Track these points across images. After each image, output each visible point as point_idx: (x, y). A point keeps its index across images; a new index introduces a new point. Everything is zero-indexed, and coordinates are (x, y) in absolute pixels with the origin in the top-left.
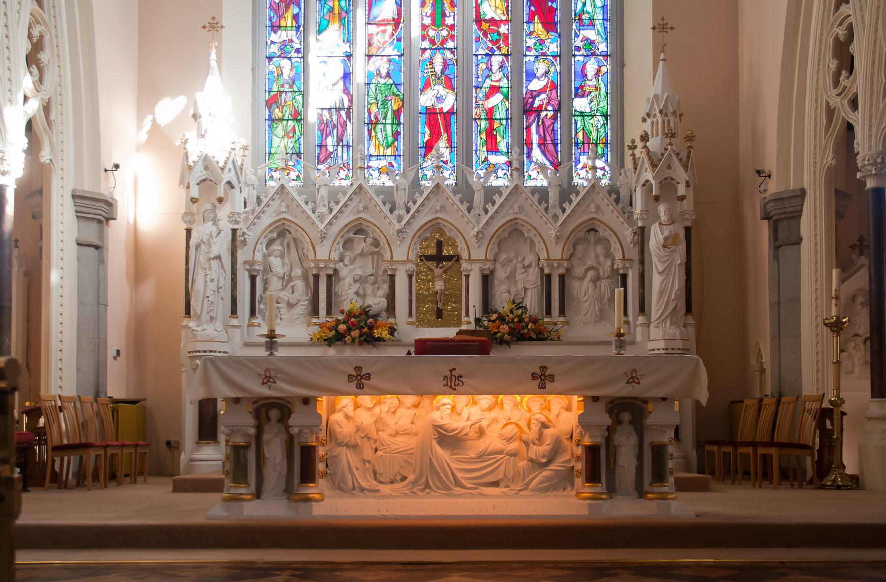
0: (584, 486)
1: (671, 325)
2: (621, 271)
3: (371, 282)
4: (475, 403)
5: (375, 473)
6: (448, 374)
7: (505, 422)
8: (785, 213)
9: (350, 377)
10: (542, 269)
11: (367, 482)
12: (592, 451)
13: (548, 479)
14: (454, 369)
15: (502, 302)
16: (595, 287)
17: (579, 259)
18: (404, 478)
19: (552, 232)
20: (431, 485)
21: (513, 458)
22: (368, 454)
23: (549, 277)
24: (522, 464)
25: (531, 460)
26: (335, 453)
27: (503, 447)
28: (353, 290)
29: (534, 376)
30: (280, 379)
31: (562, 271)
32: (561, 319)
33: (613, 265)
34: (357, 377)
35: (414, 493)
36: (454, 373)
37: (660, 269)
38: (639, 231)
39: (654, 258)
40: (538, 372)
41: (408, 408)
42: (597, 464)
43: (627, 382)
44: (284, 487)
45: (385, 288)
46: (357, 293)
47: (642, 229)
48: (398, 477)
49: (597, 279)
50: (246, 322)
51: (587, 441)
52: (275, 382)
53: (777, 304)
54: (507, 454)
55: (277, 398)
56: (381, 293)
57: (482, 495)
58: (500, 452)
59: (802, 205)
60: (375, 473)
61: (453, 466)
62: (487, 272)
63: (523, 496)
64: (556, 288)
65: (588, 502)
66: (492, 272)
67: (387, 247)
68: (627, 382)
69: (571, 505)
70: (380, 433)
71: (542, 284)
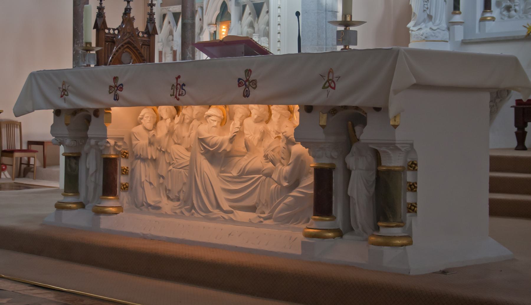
13: (289, 207)
20: (196, 206)
35: (182, 212)
50: (479, 16)
52: (67, 95)
54: (264, 175)
63: (266, 226)
68: (324, 87)
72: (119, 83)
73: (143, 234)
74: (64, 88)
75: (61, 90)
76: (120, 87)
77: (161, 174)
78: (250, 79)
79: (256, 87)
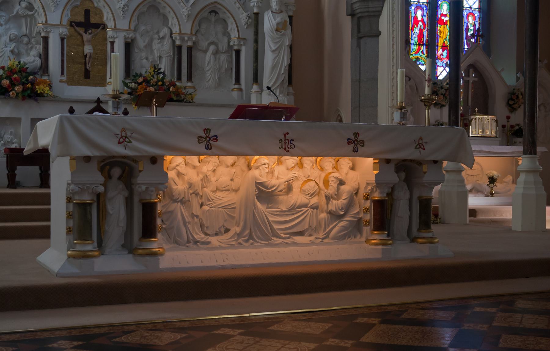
2: (236, 48)
3: (25, 42)
4: (280, 163)
5: (202, 226)
6: (282, 137)
7: (304, 179)
8: (368, 12)
9: (200, 138)
10: (174, 42)
11: (199, 236)
12: (379, 205)
13: (344, 228)
14: (288, 134)
15: (143, 66)
16: (215, 58)
17: (202, 35)
18: (227, 231)
19: (184, 10)
21: (315, 210)
22: (196, 209)
23: (180, 48)
24: (323, 215)
25: (330, 213)
26: (170, 209)
27: (307, 201)
28: (8, 49)
29: (349, 141)
31: (190, 44)
32: (189, 84)
33: (229, 42)
34: (206, 139)
36: (287, 137)
37: (274, 48)
38: (253, 16)
39: (267, 39)
40: (353, 138)
41: (228, 167)
42: (382, 215)
43: (416, 148)
44: (123, 242)
45: (39, 48)
46: (12, 52)
47: (257, 14)
48: (223, 230)
49: (216, 53)
51: (377, 196)
52: (130, 142)
53: (357, 82)
54: (311, 207)
55: (125, 157)
56: (34, 52)
57: (295, 244)
58: (305, 206)
59: (382, 7)
60: (202, 226)
61: (270, 219)
62: (129, 40)
63: (327, 244)
64: (185, 56)
65: (381, 247)
66: (133, 40)
67: (41, 11)
68: (416, 148)
69: (364, 250)
70: (205, 189)
71: (174, 54)
77: (195, 213)
78: (359, 140)
79: (364, 145)
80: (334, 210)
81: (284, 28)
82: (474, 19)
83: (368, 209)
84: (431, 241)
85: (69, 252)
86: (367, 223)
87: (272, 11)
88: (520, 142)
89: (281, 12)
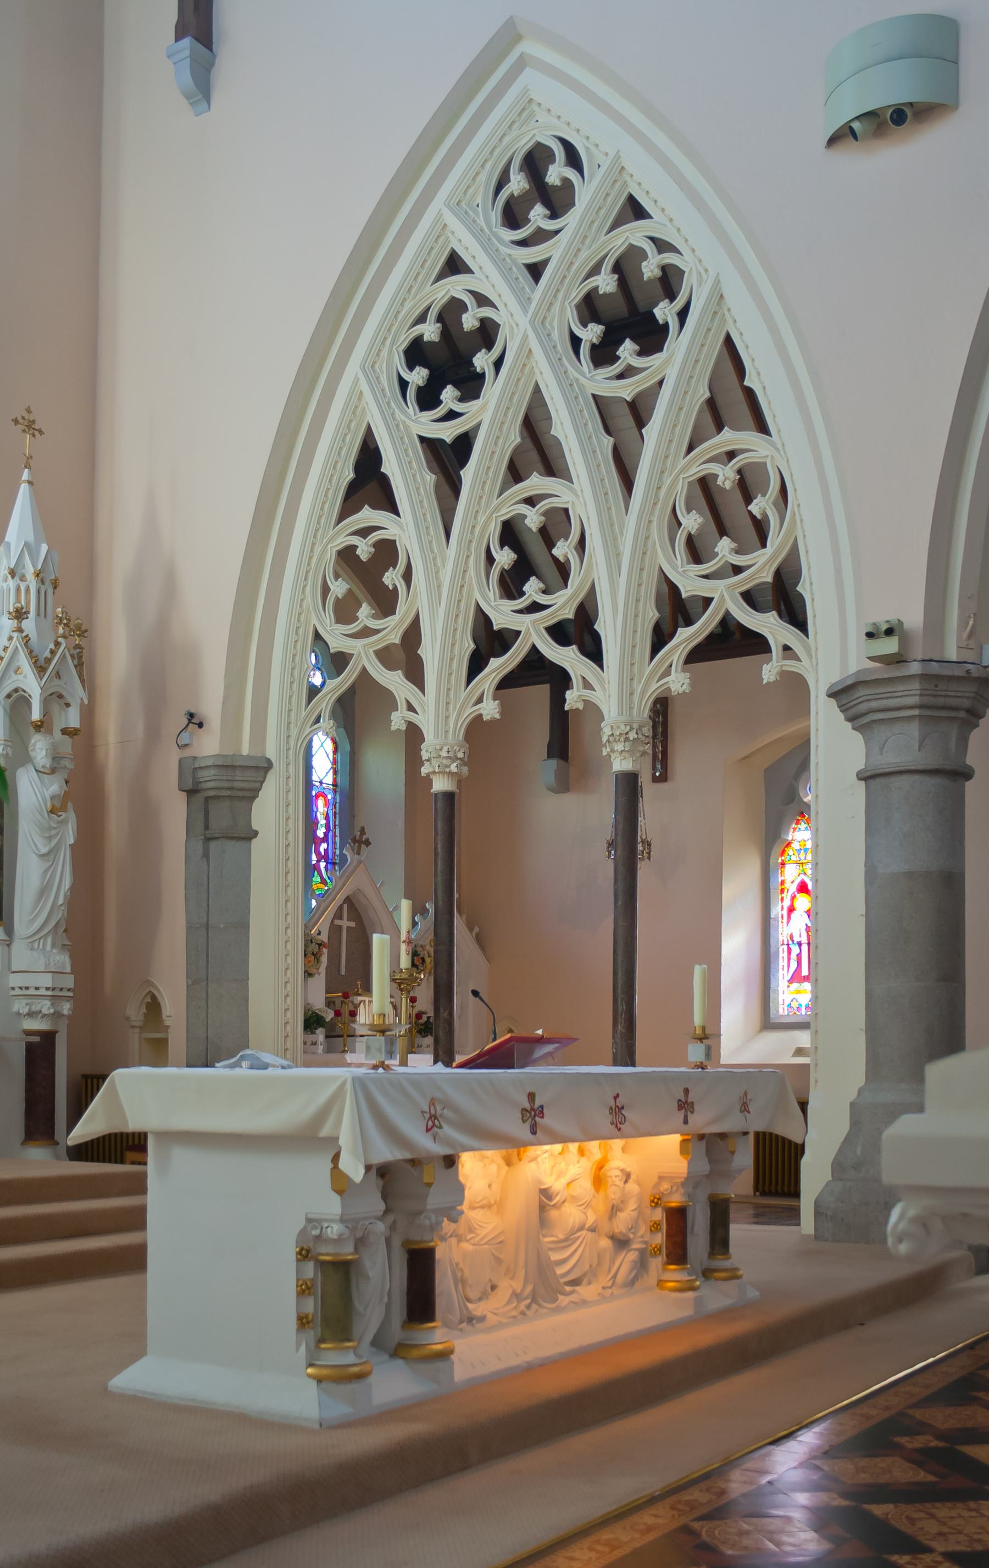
0: (664, 1270)
1: (53, 946)
14: (618, 1095)
24: (605, 1243)
30: (452, 1124)
37: (44, 850)
52: (440, 1127)
72: (538, 1103)
73: (527, 1362)
74: (433, 1112)
75: (427, 1116)
76: (540, 1112)
78: (536, 1106)
80: (624, 1231)
81: (64, 808)
82: (327, 804)
83: (658, 1225)
84: (733, 1275)
85: (310, 1370)
86: (656, 1252)
87: (37, 771)
88: (428, 1046)
89: (53, 771)
